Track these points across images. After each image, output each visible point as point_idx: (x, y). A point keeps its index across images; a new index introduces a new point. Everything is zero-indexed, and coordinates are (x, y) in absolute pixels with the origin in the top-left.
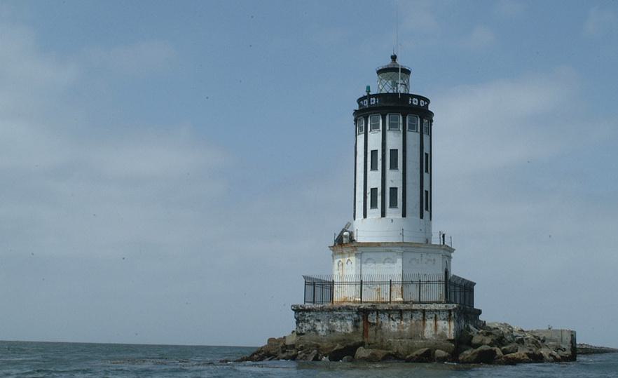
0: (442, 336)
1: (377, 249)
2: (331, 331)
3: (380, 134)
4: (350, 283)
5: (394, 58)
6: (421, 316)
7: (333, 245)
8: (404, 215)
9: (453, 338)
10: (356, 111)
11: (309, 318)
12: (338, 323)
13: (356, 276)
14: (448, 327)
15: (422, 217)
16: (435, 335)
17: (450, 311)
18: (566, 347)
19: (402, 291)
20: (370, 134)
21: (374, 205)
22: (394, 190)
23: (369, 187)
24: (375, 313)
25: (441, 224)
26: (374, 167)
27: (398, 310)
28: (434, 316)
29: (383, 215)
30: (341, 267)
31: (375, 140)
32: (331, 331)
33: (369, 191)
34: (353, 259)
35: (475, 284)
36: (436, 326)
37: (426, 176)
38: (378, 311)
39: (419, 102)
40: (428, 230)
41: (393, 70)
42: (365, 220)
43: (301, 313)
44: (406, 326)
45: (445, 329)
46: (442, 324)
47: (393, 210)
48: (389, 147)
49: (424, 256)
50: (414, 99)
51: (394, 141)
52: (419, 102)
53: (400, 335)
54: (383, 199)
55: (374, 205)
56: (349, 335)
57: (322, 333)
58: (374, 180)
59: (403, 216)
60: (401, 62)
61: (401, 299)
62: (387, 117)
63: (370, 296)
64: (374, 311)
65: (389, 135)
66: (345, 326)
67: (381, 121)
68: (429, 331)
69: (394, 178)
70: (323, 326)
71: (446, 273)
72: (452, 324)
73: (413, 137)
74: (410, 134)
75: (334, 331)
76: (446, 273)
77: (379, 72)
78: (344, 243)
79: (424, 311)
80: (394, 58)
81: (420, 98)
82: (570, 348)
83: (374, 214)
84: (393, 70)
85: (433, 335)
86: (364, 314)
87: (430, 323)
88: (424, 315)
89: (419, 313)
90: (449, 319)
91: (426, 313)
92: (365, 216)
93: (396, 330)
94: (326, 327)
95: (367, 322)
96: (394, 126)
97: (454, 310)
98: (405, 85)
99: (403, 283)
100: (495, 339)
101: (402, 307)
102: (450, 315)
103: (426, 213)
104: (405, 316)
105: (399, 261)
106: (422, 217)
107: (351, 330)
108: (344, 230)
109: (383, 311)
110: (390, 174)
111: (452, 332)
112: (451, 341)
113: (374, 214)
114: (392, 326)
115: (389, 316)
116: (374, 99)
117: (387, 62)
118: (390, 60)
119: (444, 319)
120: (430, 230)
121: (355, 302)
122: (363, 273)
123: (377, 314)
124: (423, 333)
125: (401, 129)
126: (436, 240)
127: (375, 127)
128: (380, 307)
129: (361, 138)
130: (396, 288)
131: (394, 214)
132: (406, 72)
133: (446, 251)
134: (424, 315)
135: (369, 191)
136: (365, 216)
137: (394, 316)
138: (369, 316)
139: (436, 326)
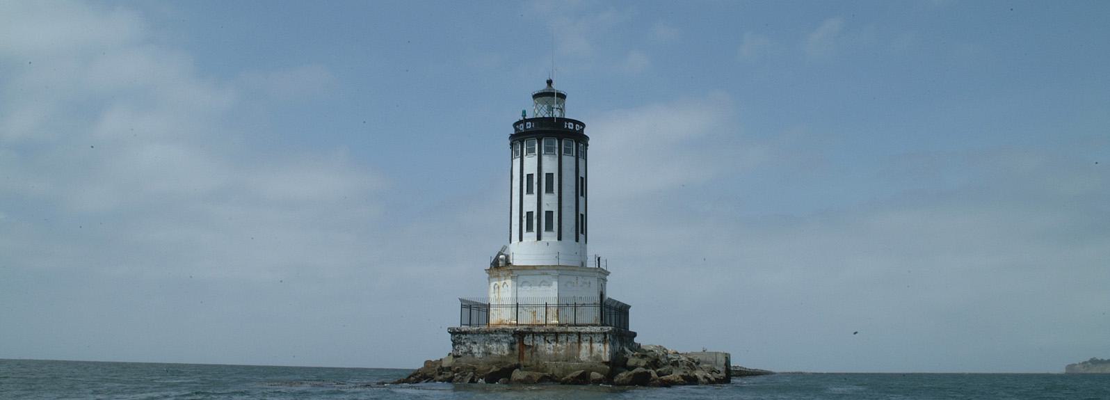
5: (550, 82)
6: (577, 338)
8: (560, 238)
11: (465, 341)
21: (529, 228)
26: (530, 191)
27: (553, 333)
29: (539, 238)
31: (531, 164)
39: (574, 126)
41: (548, 95)
43: (457, 336)
45: (600, 351)
50: (570, 123)
51: (550, 165)
52: (574, 126)
58: (530, 203)
59: (559, 240)
60: (556, 87)
62: (525, 143)
69: (550, 202)
73: (569, 161)
75: (490, 354)
77: (535, 96)
80: (550, 82)
81: (575, 122)
83: (530, 237)
84: (548, 95)
88: (580, 338)
89: (575, 335)
91: (582, 336)
92: (521, 239)
93: (552, 352)
108: (500, 253)
111: (608, 354)
113: (530, 237)
115: (545, 339)
116: (530, 123)
119: (600, 342)
123: (533, 337)
134: (580, 338)
136: (521, 239)
138: (525, 338)
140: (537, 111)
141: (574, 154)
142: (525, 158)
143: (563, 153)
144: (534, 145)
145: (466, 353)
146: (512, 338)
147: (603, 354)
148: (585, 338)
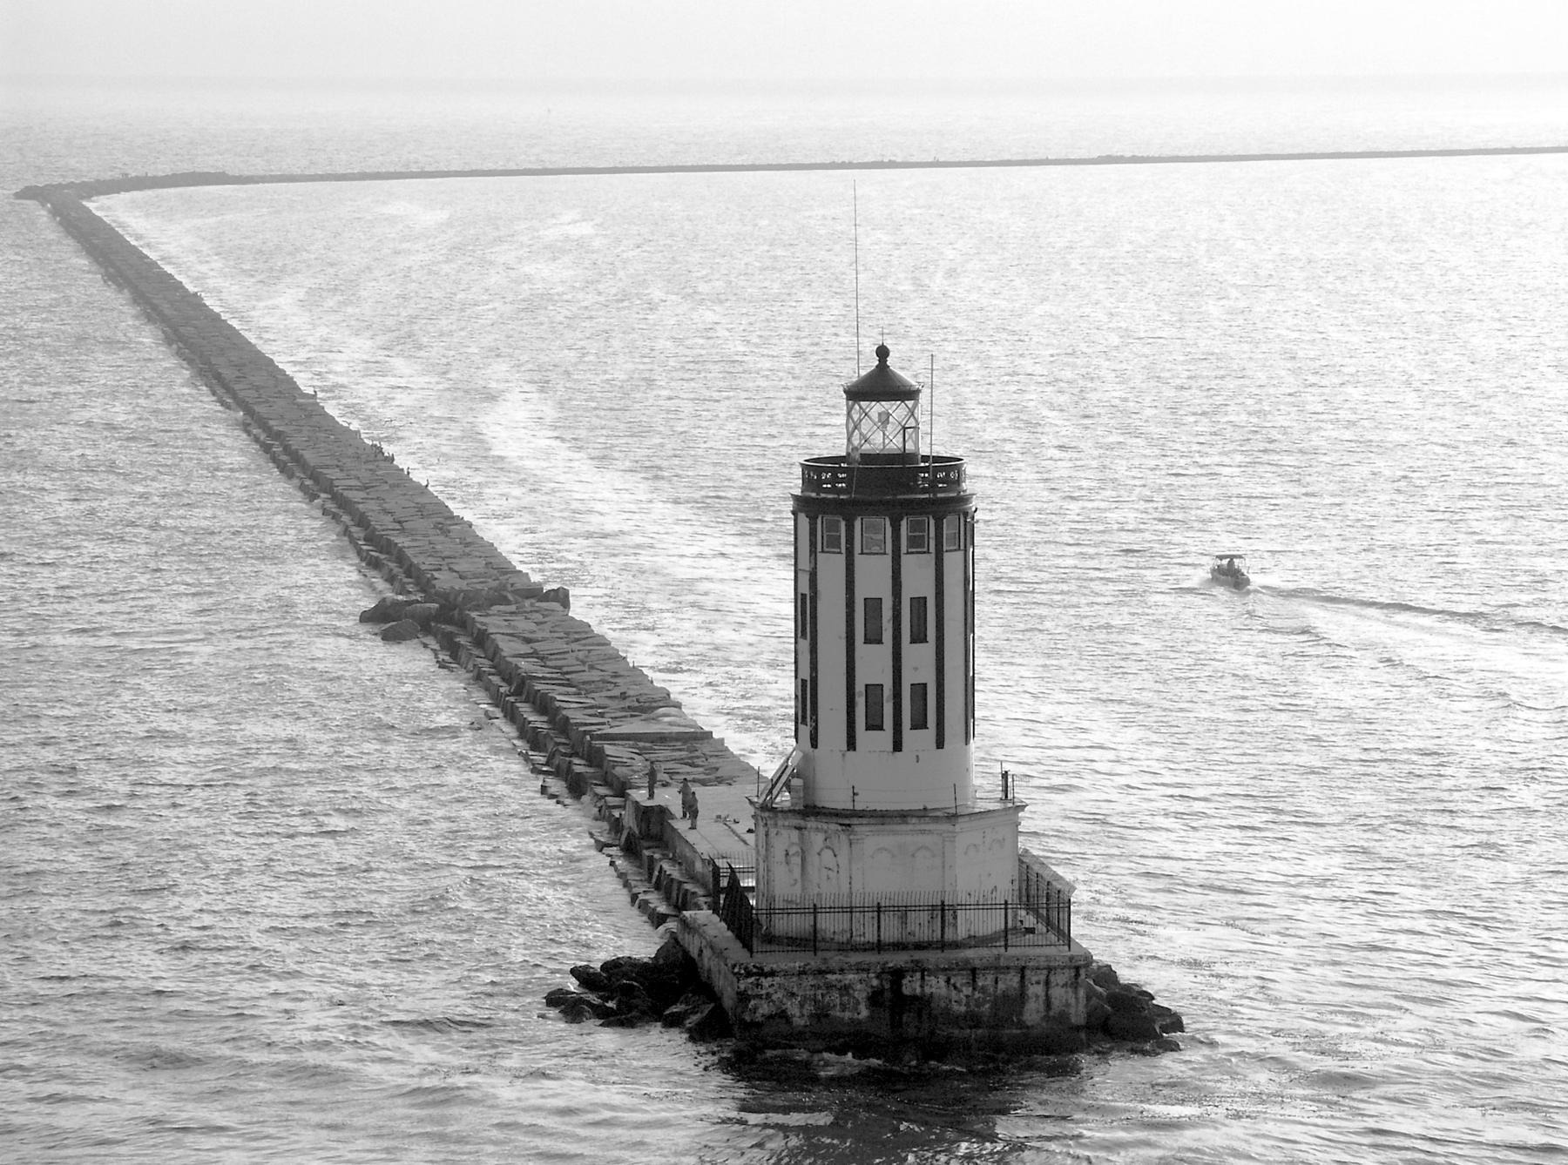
5: (883, 352)
6: (1017, 979)
10: (795, 498)
11: (771, 990)
14: (1073, 1001)
16: (1047, 1018)
21: (874, 725)
23: (928, 649)
24: (918, 975)
26: (920, 690)
28: (1043, 978)
29: (897, 746)
31: (873, 577)
36: (1048, 997)
41: (880, 386)
43: (752, 979)
44: (985, 1001)
45: (1068, 1005)
56: (860, 1022)
57: (799, 1022)
62: (904, 523)
64: (914, 971)
70: (802, 1006)
75: (827, 1016)
83: (874, 742)
85: (1043, 1019)
88: (1023, 977)
89: (1013, 973)
91: (1028, 972)
92: (851, 744)
93: (963, 1009)
100: (302, 295)
110: (909, 650)
111: (1081, 1008)
115: (948, 981)
119: (1065, 985)
123: (923, 978)
124: (1021, 1013)
134: (1023, 977)
136: (851, 744)
138: (904, 982)
139: (1048, 997)
141: (932, 549)
142: (905, 559)
143: (904, 549)
144: (838, 530)
145: (771, 1017)
146: (875, 982)
147: (1072, 1011)
148: (1034, 979)
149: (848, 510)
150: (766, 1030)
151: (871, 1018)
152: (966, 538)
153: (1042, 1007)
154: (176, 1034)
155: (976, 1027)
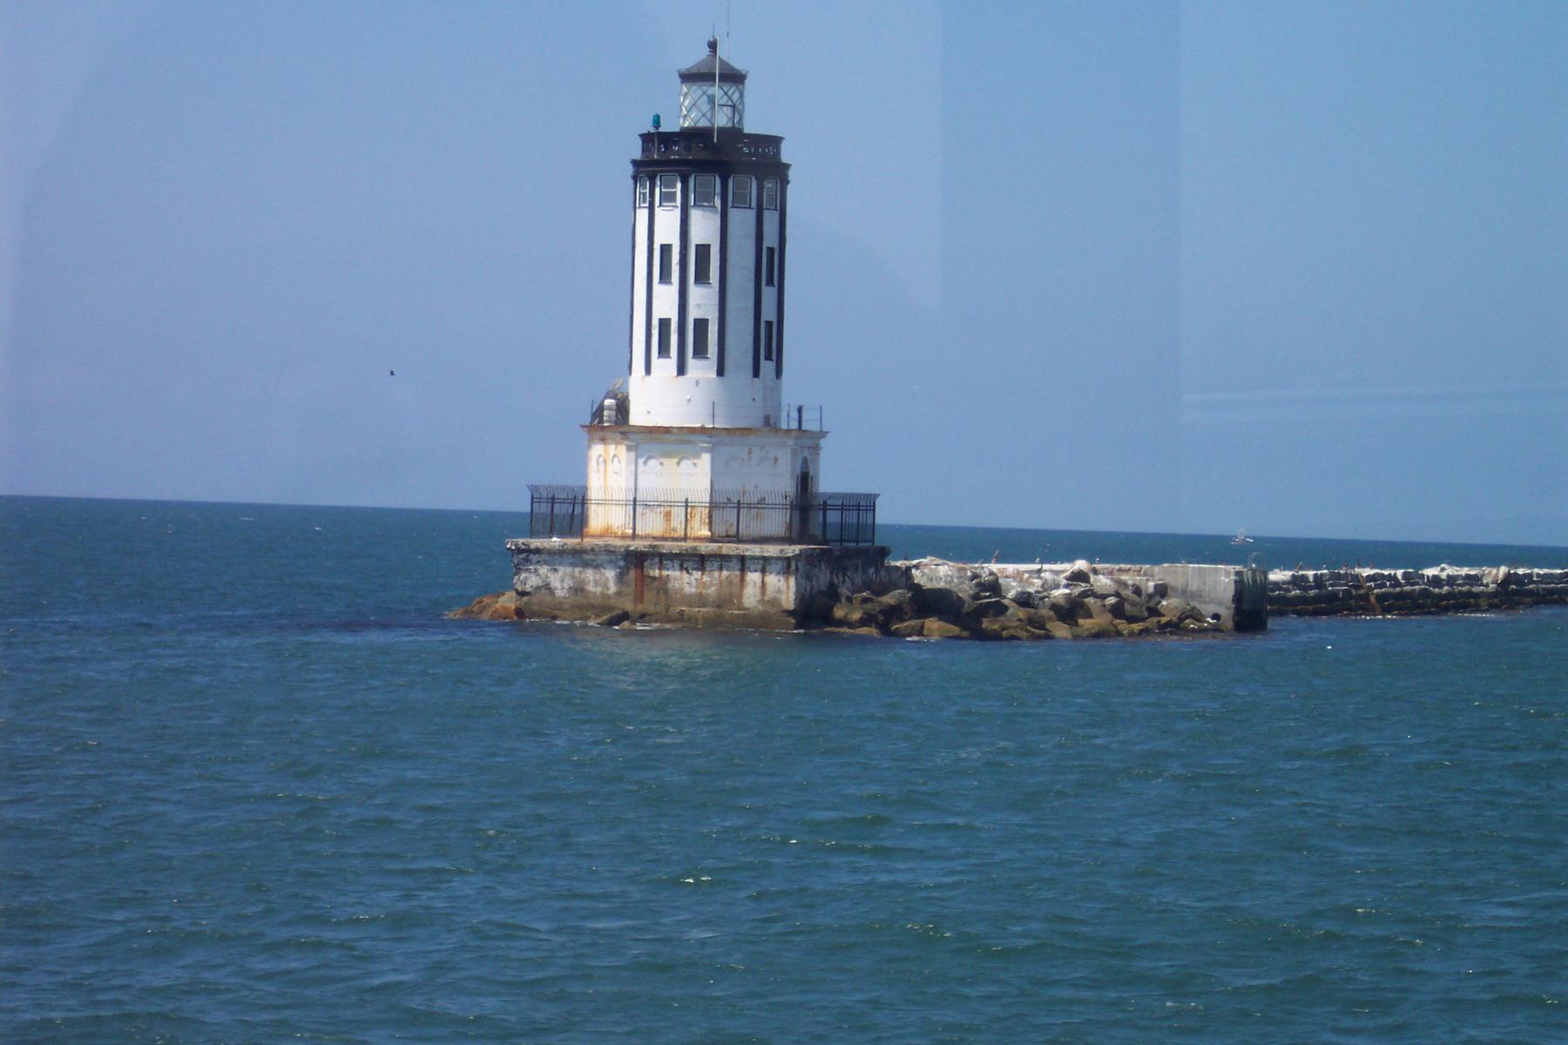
0: (774, 602)
1: (667, 437)
2: (578, 589)
3: (678, 212)
4: (618, 503)
5: (713, 46)
7: (587, 423)
9: (791, 606)
10: (635, 163)
12: (590, 574)
13: (628, 490)
14: (784, 588)
15: (756, 374)
16: (762, 601)
17: (788, 559)
18: (1222, 611)
19: (710, 517)
20: (658, 211)
21: (664, 351)
22: (701, 325)
23: (657, 314)
24: (657, 560)
25: (804, 379)
26: (665, 277)
29: (681, 370)
30: (602, 466)
32: (578, 589)
33: (655, 323)
34: (622, 449)
35: (876, 496)
36: (763, 584)
37: (769, 294)
38: (662, 557)
40: (774, 393)
42: (648, 378)
44: (711, 585)
45: (779, 591)
46: (774, 580)
47: (700, 363)
48: (696, 238)
49: (756, 453)
51: (704, 227)
53: (701, 600)
54: (685, 340)
55: (664, 351)
57: (560, 593)
58: (666, 302)
61: (706, 532)
63: (651, 525)
65: (696, 215)
66: (604, 581)
67: (679, 185)
68: (751, 596)
69: (703, 302)
70: (562, 581)
71: (805, 480)
72: (792, 581)
73: (742, 220)
74: (734, 215)
75: (582, 590)
76: (805, 480)
78: (612, 420)
79: (742, 560)
80: (713, 46)
82: (1231, 612)
86: (637, 561)
87: (753, 577)
90: (786, 571)
92: (648, 370)
93: (693, 590)
94: (568, 583)
95: (643, 579)
96: (703, 200)
97: (797, 557)
98: (734, 107)
99: (713, 506)
101: (706, 548)
102: (789, 566)
103: (767, 367)
104: (708, 565)
105: (706, 458)
106: (756, 374)
107: (613, 589)
109: (672, 557)
110: (696, 293)
111: (792, 597)
112: (790, 613)
113: (665, 367)
114: (686, 582)
117: (695, 56)
118: (706, 51)
120: (779, 398)
121: (623, 537)
122: (640, 486)
124: (740, 597)
125: (718, 202)
126: (788, 422)
127: (668, 198)
128: (668, 547)
129: (642, 215)
130: (701, 514)
131: (703, 370)
132: (734, 78)
133: (808, 442)
135: (655, 323)
136: (648, 370)
137: (689, 564)
139: (763, 584)
140: (686, 110)
145: (538, 588)
147: (783, 597)
149: (683, 168)
150: (534, 600)
151: (618, 593)
152: (784, 182)
153: (758, 591)
154: (911, 870)
155: (704, 606)
